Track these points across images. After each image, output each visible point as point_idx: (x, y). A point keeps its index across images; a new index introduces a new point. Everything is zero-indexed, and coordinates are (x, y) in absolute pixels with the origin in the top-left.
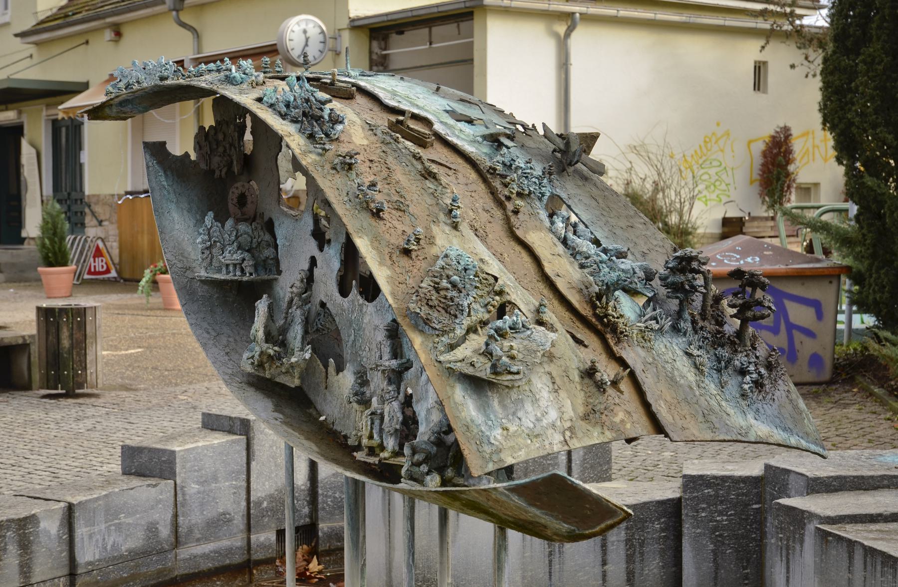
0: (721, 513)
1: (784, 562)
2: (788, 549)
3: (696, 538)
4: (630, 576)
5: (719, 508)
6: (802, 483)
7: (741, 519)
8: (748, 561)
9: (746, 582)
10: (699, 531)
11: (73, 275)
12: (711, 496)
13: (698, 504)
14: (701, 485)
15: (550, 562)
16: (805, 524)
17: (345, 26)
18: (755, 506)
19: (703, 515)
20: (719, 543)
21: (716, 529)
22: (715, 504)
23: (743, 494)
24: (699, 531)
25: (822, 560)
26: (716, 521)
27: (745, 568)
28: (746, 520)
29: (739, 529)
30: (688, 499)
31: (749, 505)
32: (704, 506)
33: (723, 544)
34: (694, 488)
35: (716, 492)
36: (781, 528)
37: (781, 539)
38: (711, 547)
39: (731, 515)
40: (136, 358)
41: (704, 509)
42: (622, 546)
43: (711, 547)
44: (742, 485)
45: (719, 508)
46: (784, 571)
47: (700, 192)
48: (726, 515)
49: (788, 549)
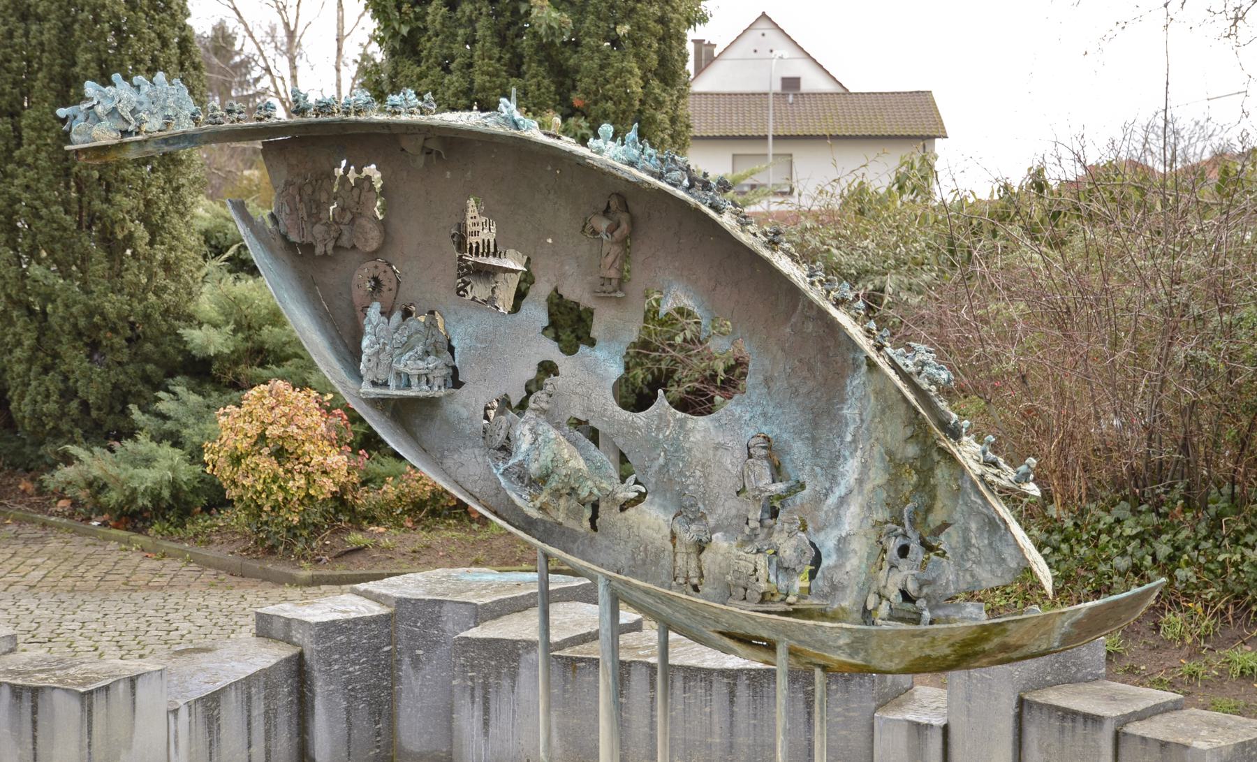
0: (353, 663)
1: (28, 726)
2: (486, 687)
3: (329, 697)
4: (268, 752)
5: (352, 656)
6: (465, 612)
7: (373, 666)
8: (380, 714)
9: (378, 739)
10: (332, 687)
11: (493, 502)
12: (343, 644)
13: (330, 656)
14: (333, 632)
15: (210, 753)
16: (519, 655)
17: (303, 87)
18: (386, 649)
19: (336, 667)
20: (351, 697)
21: (349, 682)
22: (348, 653)
23: (375, 637)
24: (332, 687)
25: (565, 691)
26: (349, 672)
27: (377, 723)
28: (378, 666)
29: (371, 679)
30: (320, 652)
31: (381, 648)
32: (337, 656)
33: (356, 698)
34: (326, 637)
35: (349, 638)
36: (472, 666)
37: (472, 679)
38: (344, 704)
39: (363, 663)
40: (587, 585)
41: (336, 660)
42: (262, 718)
43: (344, 704)
44: (373, 626)
45: (352, 656)
46: (478, 713)
47: (68, 187)
48: (359, 664)
49: (486, 687)
